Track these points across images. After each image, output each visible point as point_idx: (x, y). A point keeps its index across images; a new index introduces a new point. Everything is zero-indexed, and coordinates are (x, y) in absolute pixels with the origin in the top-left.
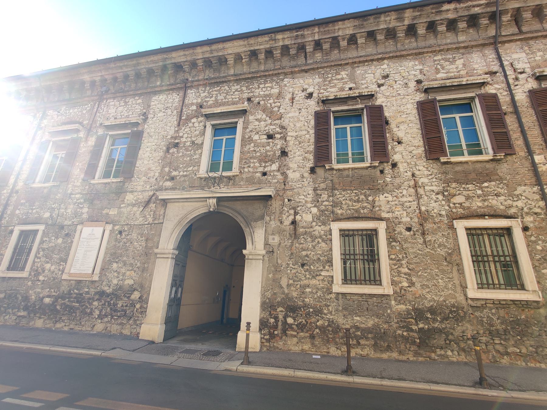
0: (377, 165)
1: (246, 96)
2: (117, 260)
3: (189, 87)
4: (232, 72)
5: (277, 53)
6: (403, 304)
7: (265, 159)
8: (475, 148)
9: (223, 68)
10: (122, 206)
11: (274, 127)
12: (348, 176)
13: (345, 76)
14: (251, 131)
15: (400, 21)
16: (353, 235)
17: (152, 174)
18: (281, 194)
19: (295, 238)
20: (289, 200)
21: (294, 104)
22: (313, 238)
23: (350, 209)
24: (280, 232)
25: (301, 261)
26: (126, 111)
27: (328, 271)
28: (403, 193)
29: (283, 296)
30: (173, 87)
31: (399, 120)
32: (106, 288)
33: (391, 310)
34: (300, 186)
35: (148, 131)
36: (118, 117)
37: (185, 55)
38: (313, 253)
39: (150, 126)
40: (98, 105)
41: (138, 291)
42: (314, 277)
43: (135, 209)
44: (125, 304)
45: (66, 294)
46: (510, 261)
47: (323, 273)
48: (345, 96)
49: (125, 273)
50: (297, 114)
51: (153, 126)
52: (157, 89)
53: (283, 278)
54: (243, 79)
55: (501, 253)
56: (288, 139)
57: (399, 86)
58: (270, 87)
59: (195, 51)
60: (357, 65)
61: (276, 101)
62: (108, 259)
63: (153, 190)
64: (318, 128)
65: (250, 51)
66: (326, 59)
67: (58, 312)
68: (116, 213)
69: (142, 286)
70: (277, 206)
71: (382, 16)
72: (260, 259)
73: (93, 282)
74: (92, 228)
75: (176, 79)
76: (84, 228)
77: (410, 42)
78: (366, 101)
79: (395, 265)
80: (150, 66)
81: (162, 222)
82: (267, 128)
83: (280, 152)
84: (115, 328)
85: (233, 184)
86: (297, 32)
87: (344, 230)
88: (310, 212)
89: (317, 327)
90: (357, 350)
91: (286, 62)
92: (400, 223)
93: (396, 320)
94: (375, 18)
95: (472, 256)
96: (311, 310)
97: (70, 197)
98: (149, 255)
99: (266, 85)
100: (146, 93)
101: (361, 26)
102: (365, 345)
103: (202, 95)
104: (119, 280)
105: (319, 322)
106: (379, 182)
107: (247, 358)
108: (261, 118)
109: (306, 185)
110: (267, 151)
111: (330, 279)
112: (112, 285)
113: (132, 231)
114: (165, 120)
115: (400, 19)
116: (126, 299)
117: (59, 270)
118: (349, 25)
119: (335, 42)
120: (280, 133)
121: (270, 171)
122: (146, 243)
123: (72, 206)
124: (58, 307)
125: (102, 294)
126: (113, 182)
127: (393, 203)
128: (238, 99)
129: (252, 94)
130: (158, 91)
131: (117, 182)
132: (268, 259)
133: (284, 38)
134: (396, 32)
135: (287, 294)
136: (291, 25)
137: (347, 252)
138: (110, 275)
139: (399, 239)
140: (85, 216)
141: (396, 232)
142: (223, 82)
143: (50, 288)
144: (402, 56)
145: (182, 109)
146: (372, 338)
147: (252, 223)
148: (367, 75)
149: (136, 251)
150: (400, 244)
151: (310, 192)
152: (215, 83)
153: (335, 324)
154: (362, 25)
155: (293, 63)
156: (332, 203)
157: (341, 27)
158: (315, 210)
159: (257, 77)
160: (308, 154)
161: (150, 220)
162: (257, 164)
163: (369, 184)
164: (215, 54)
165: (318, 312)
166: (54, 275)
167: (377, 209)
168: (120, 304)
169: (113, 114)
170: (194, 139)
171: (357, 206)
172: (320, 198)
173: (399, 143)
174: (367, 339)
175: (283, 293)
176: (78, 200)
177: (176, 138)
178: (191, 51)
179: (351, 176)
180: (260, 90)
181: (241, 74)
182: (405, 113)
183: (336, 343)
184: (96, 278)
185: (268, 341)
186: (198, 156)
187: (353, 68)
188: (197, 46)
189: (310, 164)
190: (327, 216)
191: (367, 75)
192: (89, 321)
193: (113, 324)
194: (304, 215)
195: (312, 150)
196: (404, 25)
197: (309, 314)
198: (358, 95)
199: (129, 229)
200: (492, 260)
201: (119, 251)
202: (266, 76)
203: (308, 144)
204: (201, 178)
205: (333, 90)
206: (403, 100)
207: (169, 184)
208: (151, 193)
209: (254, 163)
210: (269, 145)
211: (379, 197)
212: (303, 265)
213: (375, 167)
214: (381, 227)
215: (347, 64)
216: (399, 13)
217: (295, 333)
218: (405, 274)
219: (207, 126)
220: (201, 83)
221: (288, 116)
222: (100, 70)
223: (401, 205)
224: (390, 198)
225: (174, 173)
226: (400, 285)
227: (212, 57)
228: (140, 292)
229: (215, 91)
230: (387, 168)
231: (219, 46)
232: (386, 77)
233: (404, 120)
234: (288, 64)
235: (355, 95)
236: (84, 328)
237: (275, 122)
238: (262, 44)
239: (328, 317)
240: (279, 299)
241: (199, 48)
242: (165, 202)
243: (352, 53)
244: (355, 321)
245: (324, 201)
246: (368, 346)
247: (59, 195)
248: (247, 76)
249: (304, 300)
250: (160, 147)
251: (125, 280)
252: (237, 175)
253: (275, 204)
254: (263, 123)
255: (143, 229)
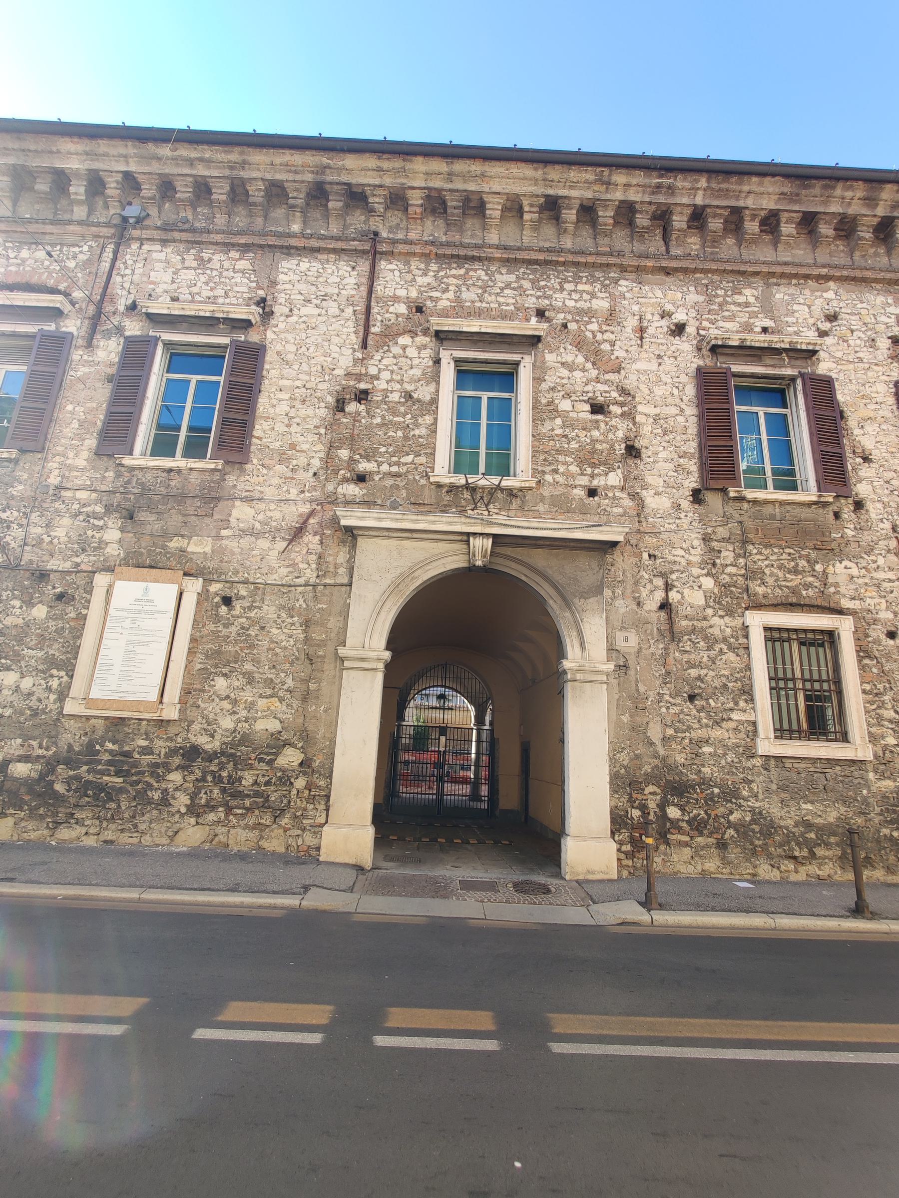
0: (831, 500)
1: (531, 302)
2: (225, 670)
3: (382, 253)
4: (493, 237)
5: (606, 215)
6: (889, 778)
7: (589, 458)
8: (787, 479)
9: (469, 223)
10: (224, 533)
11: (606, 388)
12: (772, 517)
13: (752, 300)
14: (552, 389)
15: (868, 206)
16: (789, 640)
17: (302, 460)
18: (634, 542)
19: (673, 639)
20: (650, 556)
21: (648, 341)
22: (710, 642)
23: (780, 587)
24: (639, 624)
25: (687, 689)
26: (207, 283)
27: (745, 711)
28: (879, 563)
29: (656, 761)
30: (339, 245)
31: (864, 413)
32: (203, 741)
33: (869, 791)
34: (673, 527)
35: (279, 347)
36: (181, 297)
37: (379, 169)
38: (711, 673)
39: (283, 336)
40: (116, 253)
41: (295, 746)
42: (717, 723)
43: (264, 544)
44: (262, 780)
45: (79, 753)
46: (829, 691)
47: (735, 716)
48: (762, 345)
49: (253, 703)
50: (654, 367)
51: (290, 337)
52: (293, 242)
53: (651, 725)
54: (524, 261)
55: (816, 677)
56: (639, 418)
57: (858, 342)
58: (588, 293)
59: (408, 166)
60: (775, 280)
61: (605, 328)
62: (199, 666)
63: (311, 501)
64: (707, 406)
65: (547, 196)
66: (712, 253)
67: (59, 799)
68: (208, 549)
69: (306, 738)
70: (626, 568)
71: (840, 185)
72: (601, 682)
73: (162, 723)
74: (145, 584)
75: (345, 227)
76: (118, 584)
77: (876, 254)
78: (799, 363)
79: (871, 703)
80: (278, 177)
81: (345, 580)
82: (589, 388)
83: (623, 446)
84: (240, 837)
85: (521, 508)
86: (661, 177)
87: (770, 629)
88: (700, 587)
89: (730, 825)
90: (810, 867)
91: (620, 240)
92: (875, 621)
93: (878, 810)
94: (825, 187)
95: (770, 679)
96: (716, 791)
97: (57, 497)
98: (319, 658)
99: (580, 287)
100: (261, 246)
101: (793, 198)
102: (825, 857)
103: (421, 280)
104: (239, 721)
105: (734, 816)
106: (834, 535)
107: (589, 890)
108: (573, 362)
109: (685, 527)
110: (594, 441)
111: (751, 728)
112: (220, 731)
113: (263, 600)
114: (323, 328)
115: (870, 201)
116: (263, 766)
117: (49, 689)
118: (771, 190)
119: (735, 220)
120: (622, 405)
121: (606, 488)
122: (305, 631)
123: (66, 521)
124: (59, 787)
125: (192, 753)
126: (191, 469)
127: (861, 581)
128: (512, 308)
129: (547, 302)
130: (296, 248)
131: (203, 471)
132: (616, 681)
133: (629, 185)
134: (856, 225)
135: (664, 759)
136: (653, 158)
137: (781, 674)
138: (211, 708)
139: (877, 654)
140: (113, 551)
141: (870, 639)
142: (473, 259)
143: (26, 738)
144: (864, 280)
145: (368, 309)
146: (837, 844)
147: (576, 601)
148: (796, 307)
149: (278, 650)
150: (878, 662)
151: (696, 543)
152: (453, 256)
153: (765, 819)
154: (797, 195)
155: (638, 247)
156: (743, 571)
157: (754, 188)
158: (708, 583)
159: (557, 263)
160: (686, 460)
161: (310, 575)
162: (574, 468)
163: (813, 538)
164: (460, 186)
165: (731, 794)
166: (34, 703)
167: (832, 590)
168: (248, 778)
169: (165, 286)
170: (409, 387)
171: (795, 580)
172: (719, 558)
173: (866, 459)
174: (828, 845)
175: (656, 756)
176: (84, 505)
177: (359, 377)
178: (397, 163)
179: (778, 517)
180: (569, 296)
181: (519, 249)
182: (874, 401)
183: (770, 856)
184: (171, 712)
185: (630, 855)
186: (423, 431)
187: (768, 285)
188: (415, 154)
189: (692, 482)
190: (737, 598)
191: (796, 307)
192: (160, 820)
193: (234, 827)
194: (686, 592)
195: (692, 451)
196: (875, 216)
197: (712, 799)
198: (788, 346)
199: (252, 595)
200: (801, 686)
201: (230, 648)
202: (577, 264)
203: (684, 437)
204: (439, 486)
205: (728, 325)
206: (870, 374)
207: (353, 490)
208: (306, 508)
209: (565, 463)
210: (598, 428)
211: (834, 566)
212: (692, 698)
213: (825, 505)
214: (845, 628)
215: (756, 274)
216: (872, 188)
217: (687, 839)
218: (890, 721)
219: (444, 362)
220: (418, 249)
221: (634, 367)
222: (125, 157)
223: (875, 585)
224: (855, 571)
225: (364, 466)
226: (882, 742)
227: (451, 190)
228: (303, 750)
229: (454, 276)
230: (846, 510)
231: (473, 168)
232: (832, 318)
233: (872, 414)
234: (626, 247)
235: (783, 346)
236: (147, 837)
237: (607, 377)
238: (576, 187)
239: (749, 803)
240: (647, 769)
241: (420, 159)
242: (351, 534)
243: (764, 253)
244: (804, 812)
245: (727, 565)
246: (831, 859)
247: (21, 487)
248: (534, 256)
249: (700, 771)
250: (318, 394)
251: (255, 719)
252: (530, 489)
253: (622, 562)
254: (578, 374)
255: (291, 595)
